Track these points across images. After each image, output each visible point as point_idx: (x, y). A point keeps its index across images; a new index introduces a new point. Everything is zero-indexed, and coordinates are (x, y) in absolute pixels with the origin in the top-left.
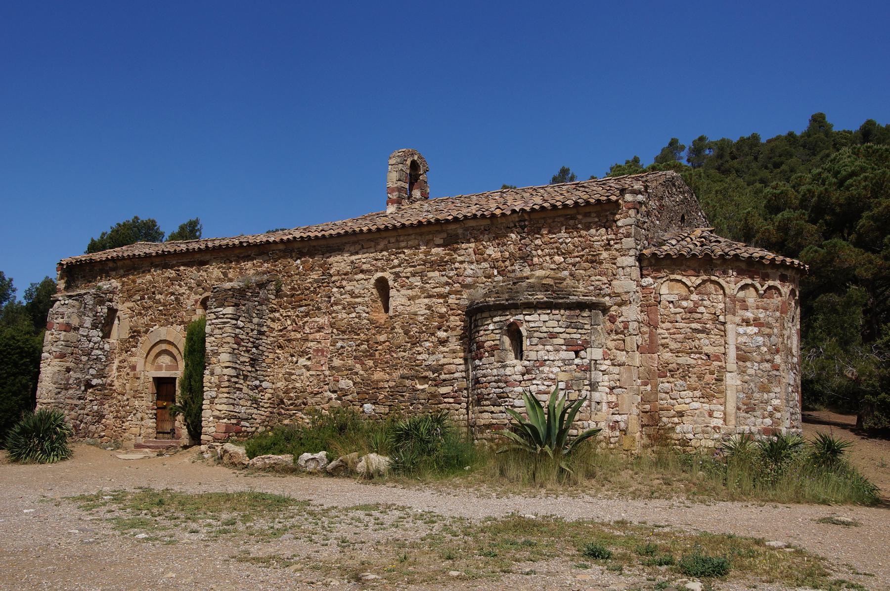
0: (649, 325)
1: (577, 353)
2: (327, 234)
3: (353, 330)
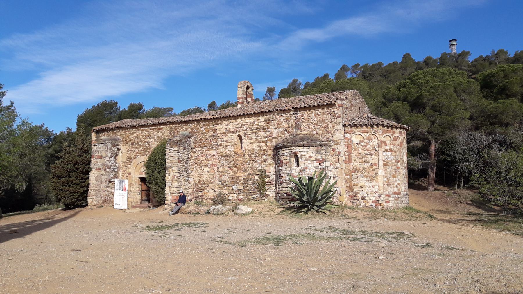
0: (348, 152)
1: (320, 164)
2: (215, 117)
3: (228, 156)
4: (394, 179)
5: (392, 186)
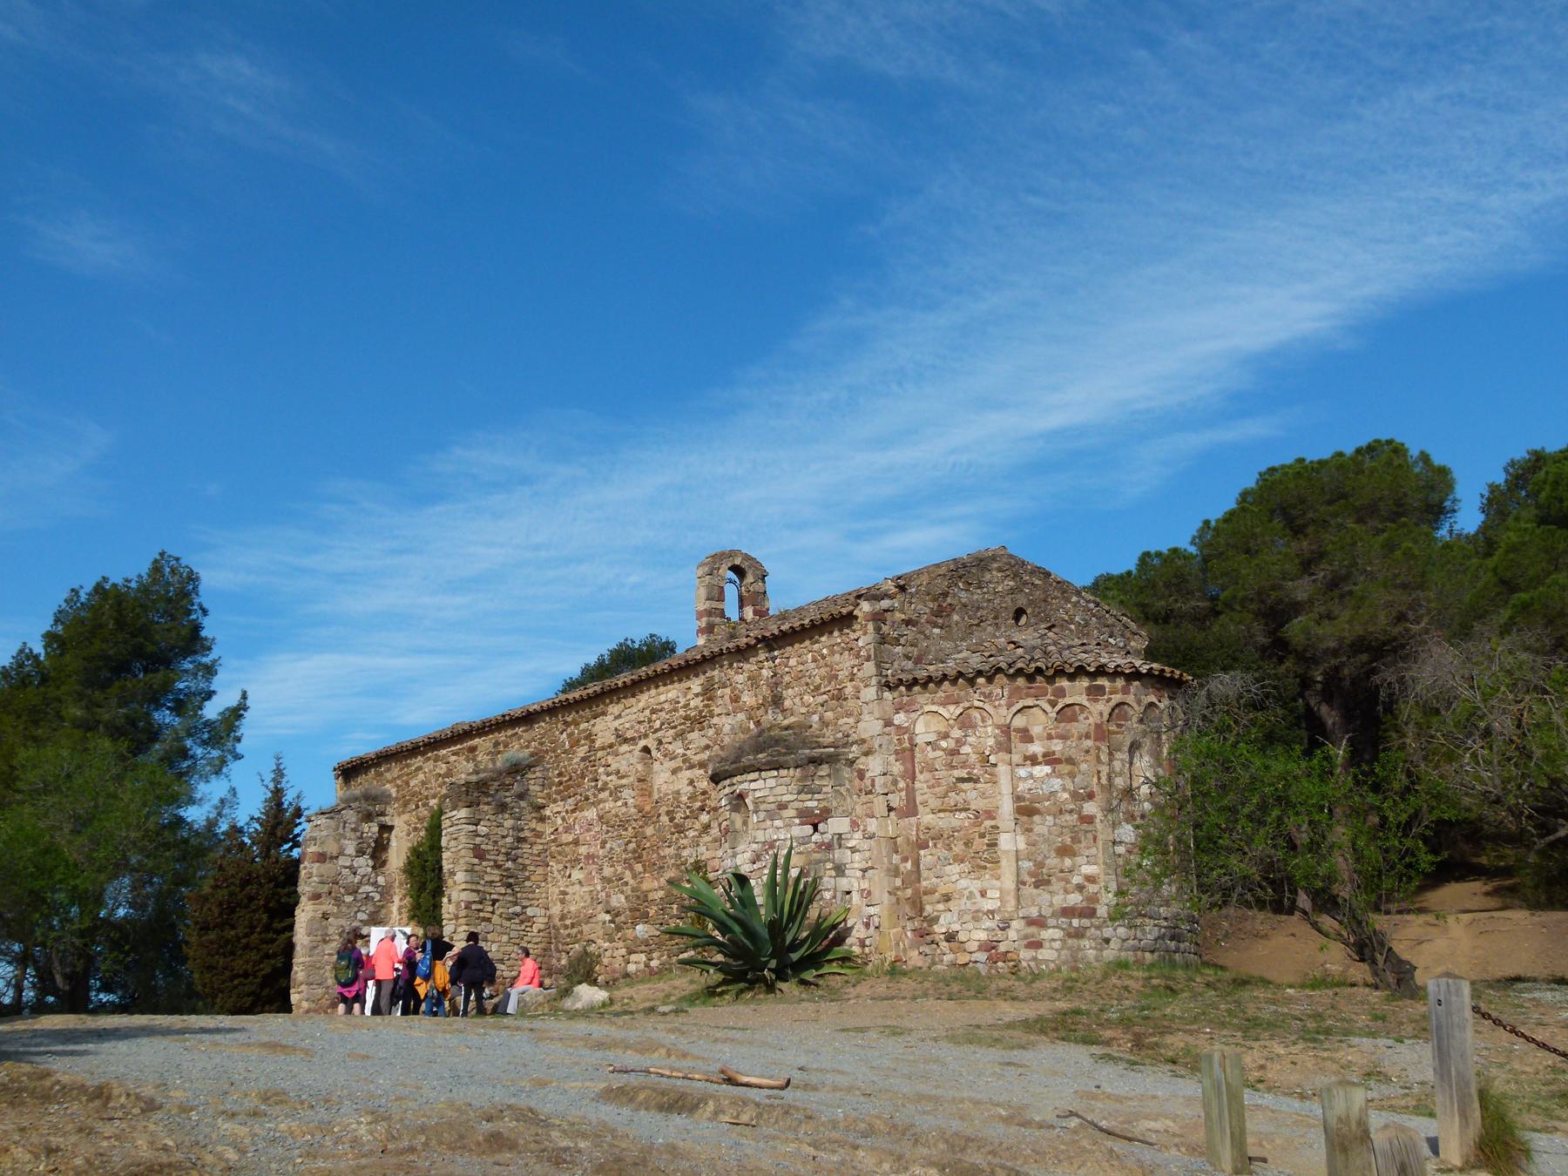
4: (1068, 862)
5: (1056, 885)
